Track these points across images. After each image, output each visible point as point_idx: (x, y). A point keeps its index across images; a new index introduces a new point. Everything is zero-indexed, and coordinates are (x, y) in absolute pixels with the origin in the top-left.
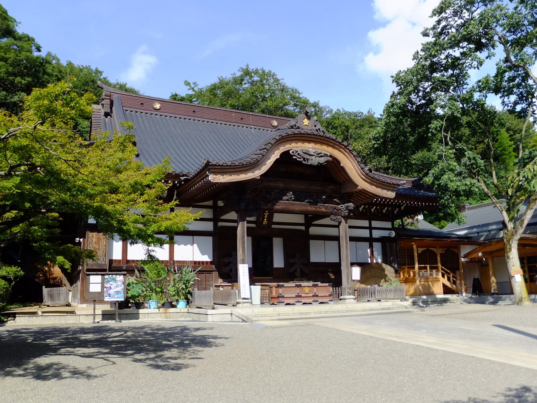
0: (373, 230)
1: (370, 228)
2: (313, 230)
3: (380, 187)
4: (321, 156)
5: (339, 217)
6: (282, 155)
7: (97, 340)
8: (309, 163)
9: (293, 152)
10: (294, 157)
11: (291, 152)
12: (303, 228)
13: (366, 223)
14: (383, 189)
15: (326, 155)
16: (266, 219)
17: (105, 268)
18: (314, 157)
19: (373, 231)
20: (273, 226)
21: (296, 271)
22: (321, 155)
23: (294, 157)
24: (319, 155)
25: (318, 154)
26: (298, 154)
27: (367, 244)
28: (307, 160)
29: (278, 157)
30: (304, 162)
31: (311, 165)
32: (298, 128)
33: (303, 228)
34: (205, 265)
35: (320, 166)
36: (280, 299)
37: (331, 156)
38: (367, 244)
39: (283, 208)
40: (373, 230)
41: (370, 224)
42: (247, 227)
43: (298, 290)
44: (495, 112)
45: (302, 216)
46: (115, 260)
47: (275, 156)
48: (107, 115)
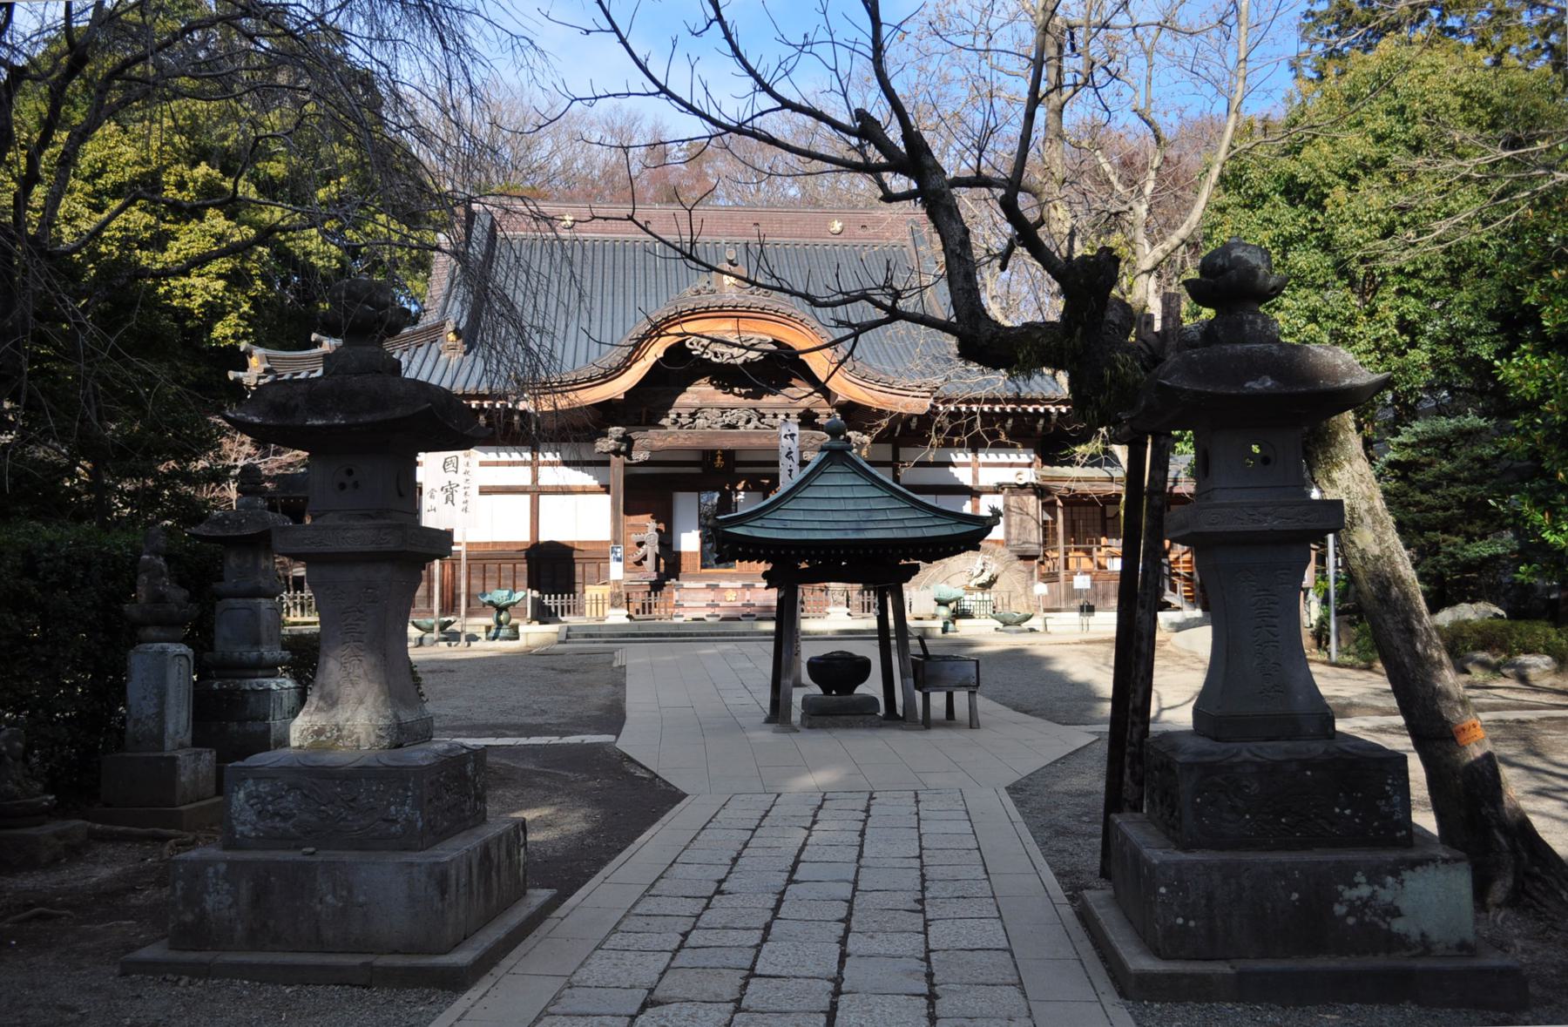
19: (982, 470)
21: (645, 558)
32: (713, 292)
37: (775, 342)
43: (711, 595)
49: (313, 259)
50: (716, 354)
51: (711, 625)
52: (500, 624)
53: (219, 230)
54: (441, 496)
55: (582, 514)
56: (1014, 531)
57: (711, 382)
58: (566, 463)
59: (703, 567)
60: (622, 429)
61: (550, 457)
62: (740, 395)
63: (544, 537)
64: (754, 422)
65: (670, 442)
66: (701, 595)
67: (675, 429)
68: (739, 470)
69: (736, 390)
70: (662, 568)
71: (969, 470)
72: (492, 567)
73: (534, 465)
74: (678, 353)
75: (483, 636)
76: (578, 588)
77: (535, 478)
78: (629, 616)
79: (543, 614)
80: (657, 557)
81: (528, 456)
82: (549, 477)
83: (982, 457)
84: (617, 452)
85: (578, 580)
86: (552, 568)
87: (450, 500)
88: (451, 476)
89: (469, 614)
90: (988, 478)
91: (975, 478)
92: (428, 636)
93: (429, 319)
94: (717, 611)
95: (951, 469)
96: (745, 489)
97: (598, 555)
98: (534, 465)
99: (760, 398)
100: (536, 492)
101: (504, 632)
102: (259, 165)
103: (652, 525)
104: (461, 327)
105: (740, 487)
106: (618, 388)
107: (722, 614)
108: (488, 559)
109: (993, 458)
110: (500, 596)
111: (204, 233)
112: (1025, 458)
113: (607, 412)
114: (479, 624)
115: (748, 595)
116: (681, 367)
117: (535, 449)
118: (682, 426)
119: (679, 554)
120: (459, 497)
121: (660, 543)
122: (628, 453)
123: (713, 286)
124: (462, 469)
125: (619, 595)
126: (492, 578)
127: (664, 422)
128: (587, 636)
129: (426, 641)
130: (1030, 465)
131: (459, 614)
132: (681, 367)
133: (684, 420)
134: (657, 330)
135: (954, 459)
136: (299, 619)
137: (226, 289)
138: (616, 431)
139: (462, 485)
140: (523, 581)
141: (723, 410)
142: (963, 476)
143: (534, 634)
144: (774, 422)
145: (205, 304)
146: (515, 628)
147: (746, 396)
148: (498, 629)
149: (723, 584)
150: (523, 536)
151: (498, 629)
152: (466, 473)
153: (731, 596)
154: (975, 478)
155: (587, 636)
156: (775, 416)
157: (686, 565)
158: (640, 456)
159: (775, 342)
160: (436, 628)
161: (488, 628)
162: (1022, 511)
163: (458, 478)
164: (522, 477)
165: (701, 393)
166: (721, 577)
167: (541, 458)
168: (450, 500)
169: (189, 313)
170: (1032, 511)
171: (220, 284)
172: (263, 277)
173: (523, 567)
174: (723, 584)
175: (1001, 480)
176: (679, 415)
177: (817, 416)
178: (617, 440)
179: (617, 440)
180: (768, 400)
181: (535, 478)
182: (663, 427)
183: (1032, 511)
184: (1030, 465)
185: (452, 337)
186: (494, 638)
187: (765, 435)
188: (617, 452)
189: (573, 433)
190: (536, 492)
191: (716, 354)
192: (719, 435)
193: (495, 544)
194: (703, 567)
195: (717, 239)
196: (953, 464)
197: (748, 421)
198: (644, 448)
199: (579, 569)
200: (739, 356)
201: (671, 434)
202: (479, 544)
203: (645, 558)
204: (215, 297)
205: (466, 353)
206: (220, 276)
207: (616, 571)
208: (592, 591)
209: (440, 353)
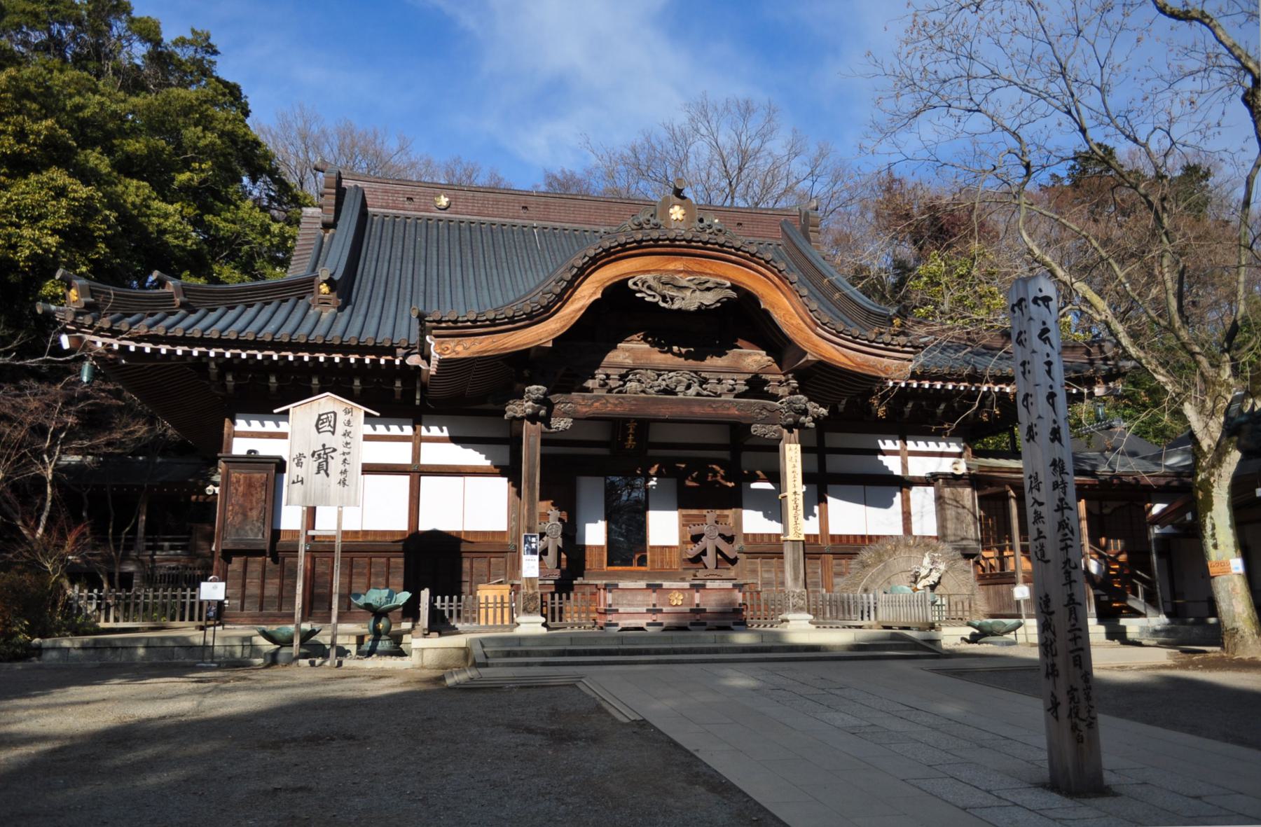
4: (709, 289)
5: (775, 427)
8: (675, 307)
9: (635, 284)
10: (638, 295)
11: (630, 283)
15: (719, 286)
16: (631, 437)
17: (262, 547)
18: (688, 293)
19: (911, 459)
21: (704, 553)
23: (638, 295)
26: (649, 288)
28: (672, 299)
29: (599, 296)
30: (662, 304)
31: (679, 310)
32: (657, 226)
35: (702, 311)
36: (609, 617)
37: (734, 287)
40: (423, 445)
42: (542, 456)
43: (653, 598)
44: (249, 156)
46: (286, 531)
47: (588, 293)
48: (326, 226)
49: (169, 238)
50: (664, 298)
51: (652, 638)
52: (377, 634)
53: (60, 182)
54: (311, 464)
55: (473, 502)
56: (950, 525)
57: (645, 340)
58: (454, 439)
59: (609, 564)
60: (543, 389)
61: (435, 431)
62: (680, 355)
63: (424, 526)
64: (695, 388)
65: (597, 408)
66: (640, 598)
67: (603, 392)
68: (651, 452)
69: (675, 348)
70: (564, 565)
71: (897, 459)
72: (361, 561)
73: (417, 441)
74: (618, 293)
75: (353, 649)
76: (466, 588)
77: (416, 454)
78: (544, 625)
79: (439, 624)
80: (560, 550)
81: (408, 430)
82: (433, 454)
83: (911, 445)
84: (533, 418)
85: (465, 578)
86: (435, 563)
87: (323, 468)
88: (326, 438)
89: (341, 619)
90: (919, 467)
91: (905, 466)
92: (285, 651)
93: (297, 270)
94: (659, 618)
95: (880, 457)
96: (658, 475)
97: (497, 551)
98: (417, 441)
99: (703, 359)
100: (416, 472)
101: (384, 644)
102: (116, 142)
103: (554, 514)
104: (337, 277)
105: (652, 472)
106: (544, 333)
107: (666, 621)
108: (363, 549)
109: (922, 446)
110: (376, 596)
111: (42, 186)
112: (955, 448)
113: (522, 366)
114: (347, 633)
115: (697, 598)
116: (621, 312)
117: (416, 423)
118: (610, 391)
119: (584, 547)
120: (335, 465)
121: (564, 535)
122: (546, 421)
123: (657, 220)
124: (340, 428)
125: (533, 597)
126: (360, 574)
127: (590, 383)
128: (508, 654)
129: (281, 658)
130: (960, 455)
131: (328, 619)
132: (621, 312)
133: (613, 383)
134: (595, 263)
135: (882, 447)
136: (111, 624)
137: (60, 246)
138: (537, 390)
139: (341, 449)
140: (399, 580)
141: (659, 372)
142: (893, 465)
143: (425, 650)
144: (719, 389)
145: (33, 257)
146: (397, 638)
147: (687, 356)
148: (376, 640)
149: (666, 585)
150: (400, 524)
151: (376, 640)
152: (346, 434)
153: (677, 599)
154: (905, 466)
155: (508, 654)
156: (720, 381)
157: (591, 562)
158: (561, 424)
159: (734, 287)
160: (297, 642)
161: (360, 640)
162: (959, 504)
163: (336, 441)
164: (400, 454)
165: (631, 351)
166: (623, 576)
167: (424, 432)
168: (323, 468)
169: (13, 265)
170: (968, 504)
171: (52, 240)
172: (106, 240)
173: (399, 561)
174: (666, 585)
175: (933, 470)
176: (608, 376)
177: (766, 382)
178: (536, 401)
179: (536, 401)
180: (713, 362)
181: (416, 454)
182: (587, 390)
183: (968, 504)
184: (960, 455)
185: (324, 288)
186: (369, 654)
187: (710, 404)
188: (533, 418)
189: (469, 401)
190: (416, 472)
191: (664, 298)
192: (655, 401)
193: (366, 533)
194: (609, 564)
195: (596, 228)
196: (883, 453)
197: (688, 387)
198: (565, 414)
199: (466, 564)
200: (690, 301)
201: (598, 398)
202: (376, 533)
203: (704, 553)
204: (46, 251)
205: (341, 309)
206: (55, 232)
207: (530, 567)
208: (488, 593)
209: (309, 307)
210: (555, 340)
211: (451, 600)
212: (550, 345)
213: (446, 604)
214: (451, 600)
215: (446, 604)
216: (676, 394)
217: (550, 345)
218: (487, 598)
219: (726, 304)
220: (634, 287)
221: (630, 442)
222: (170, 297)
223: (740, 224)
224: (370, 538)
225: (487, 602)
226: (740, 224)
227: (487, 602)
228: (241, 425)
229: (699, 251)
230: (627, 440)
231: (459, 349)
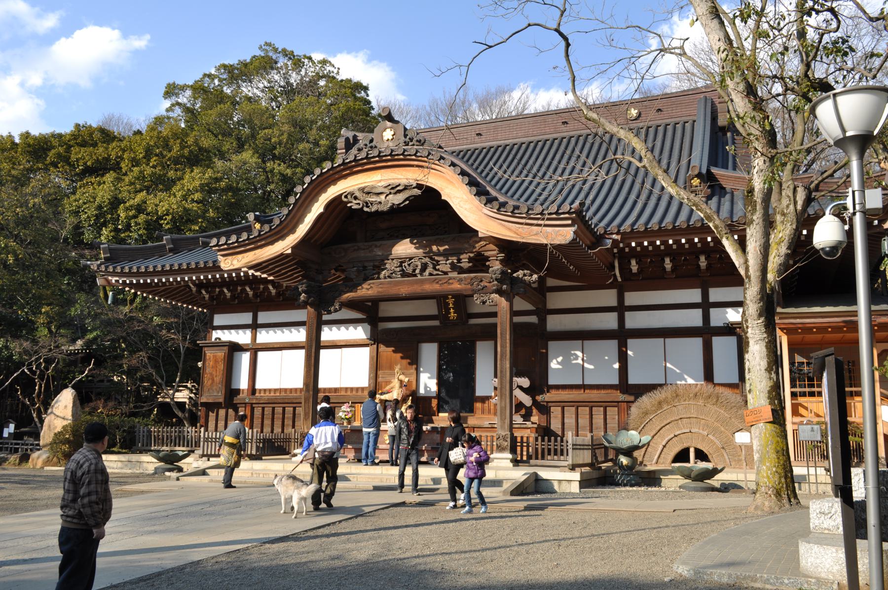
0: (712, 310)
1: (621, 309)
2: (554, 323)
3: (277, 240)
4: (399, 191)
6: (328, 206)
7: (126, 483)
12: (533, 319)
13: (694, 295)
14: (272, 243)
16: (452, 310)
18: (383, 197)
20: (473, 321)
22: (398, 188)
23: (349, 205)
24: (395, 189)
25: (393, 188)
27: (613, 344)
31: (377, 211)
33: (533, 319)
34: (354, 392)
37: (419, 186)
38: (613, 344)
39: (378, 292)
40: (712, 310)
41: (705, 295)
45: (433, 303)
47: (317, 209)
190: (622, 336)
210: (293, 248)
211: (549, 441)
212: (289, 251)
213: (552, 443)
214: (549, 441)
215: (552, 443)
216: (415, 275)
217: (289, 251)
218: (522, 438)
219: (413, 200)
220: (345, 200)
221: (453, 315)
222: (164, 245)
223: (659, 110)
224: (283, 394)
225: (522, 442)
226: (659, 110)
227: (522, 442)
228: (219, 319)
229: (389, 164)
230: (450, 313)
231: (235, 262)
